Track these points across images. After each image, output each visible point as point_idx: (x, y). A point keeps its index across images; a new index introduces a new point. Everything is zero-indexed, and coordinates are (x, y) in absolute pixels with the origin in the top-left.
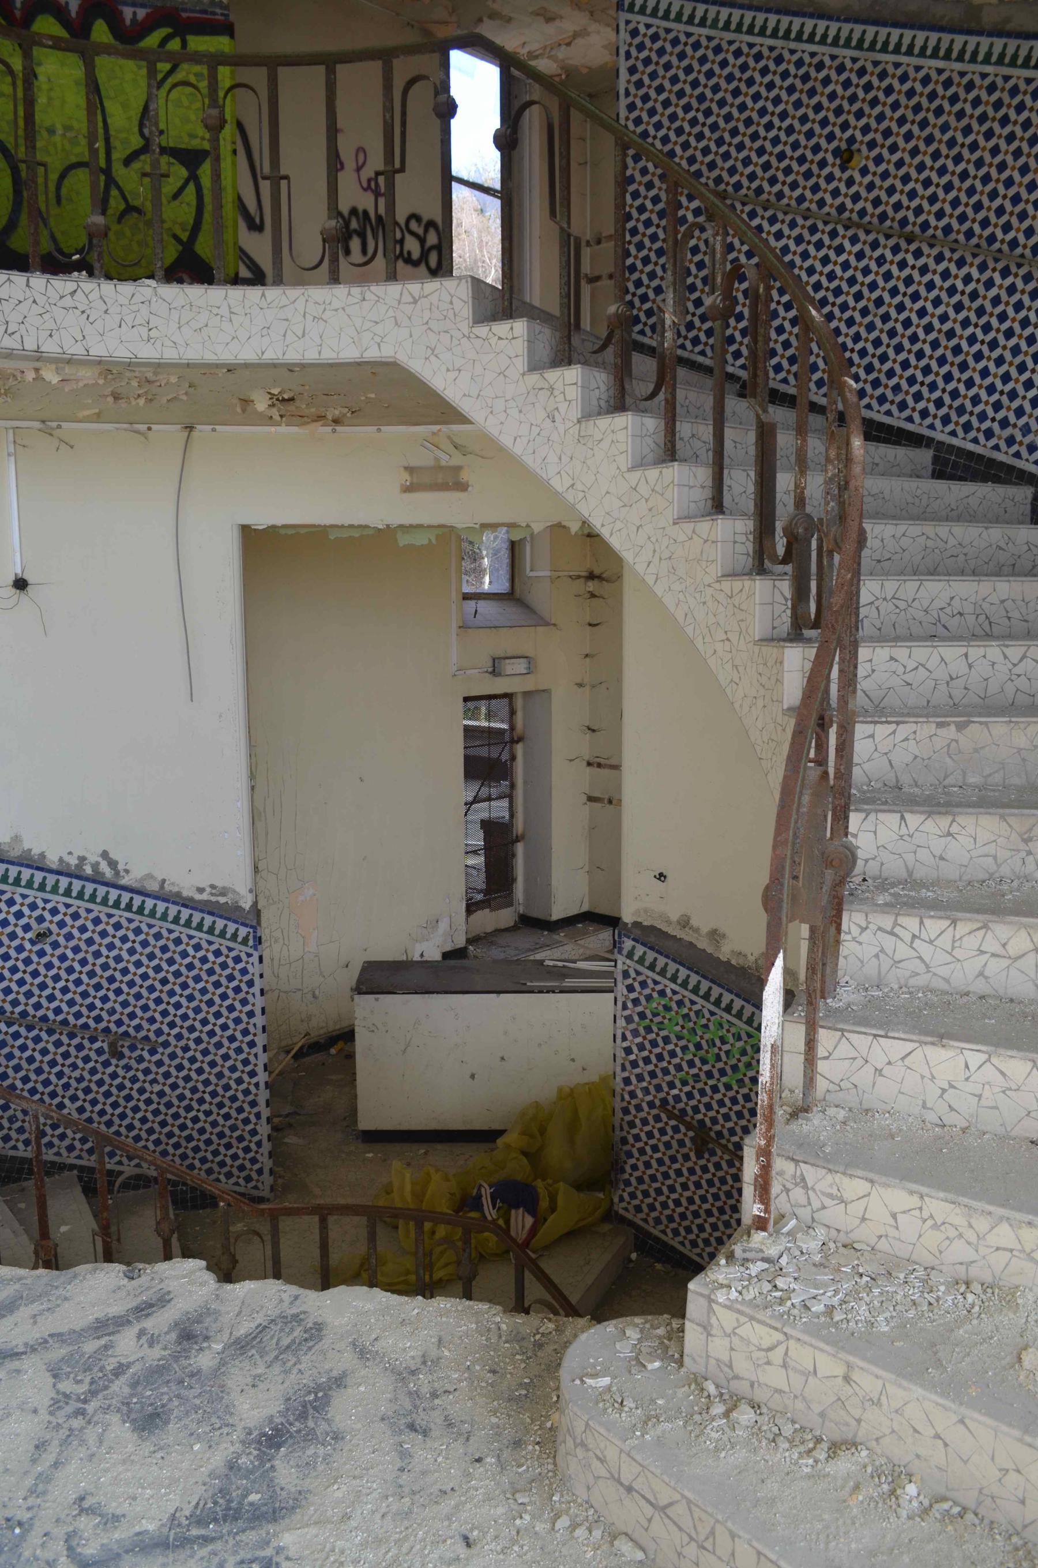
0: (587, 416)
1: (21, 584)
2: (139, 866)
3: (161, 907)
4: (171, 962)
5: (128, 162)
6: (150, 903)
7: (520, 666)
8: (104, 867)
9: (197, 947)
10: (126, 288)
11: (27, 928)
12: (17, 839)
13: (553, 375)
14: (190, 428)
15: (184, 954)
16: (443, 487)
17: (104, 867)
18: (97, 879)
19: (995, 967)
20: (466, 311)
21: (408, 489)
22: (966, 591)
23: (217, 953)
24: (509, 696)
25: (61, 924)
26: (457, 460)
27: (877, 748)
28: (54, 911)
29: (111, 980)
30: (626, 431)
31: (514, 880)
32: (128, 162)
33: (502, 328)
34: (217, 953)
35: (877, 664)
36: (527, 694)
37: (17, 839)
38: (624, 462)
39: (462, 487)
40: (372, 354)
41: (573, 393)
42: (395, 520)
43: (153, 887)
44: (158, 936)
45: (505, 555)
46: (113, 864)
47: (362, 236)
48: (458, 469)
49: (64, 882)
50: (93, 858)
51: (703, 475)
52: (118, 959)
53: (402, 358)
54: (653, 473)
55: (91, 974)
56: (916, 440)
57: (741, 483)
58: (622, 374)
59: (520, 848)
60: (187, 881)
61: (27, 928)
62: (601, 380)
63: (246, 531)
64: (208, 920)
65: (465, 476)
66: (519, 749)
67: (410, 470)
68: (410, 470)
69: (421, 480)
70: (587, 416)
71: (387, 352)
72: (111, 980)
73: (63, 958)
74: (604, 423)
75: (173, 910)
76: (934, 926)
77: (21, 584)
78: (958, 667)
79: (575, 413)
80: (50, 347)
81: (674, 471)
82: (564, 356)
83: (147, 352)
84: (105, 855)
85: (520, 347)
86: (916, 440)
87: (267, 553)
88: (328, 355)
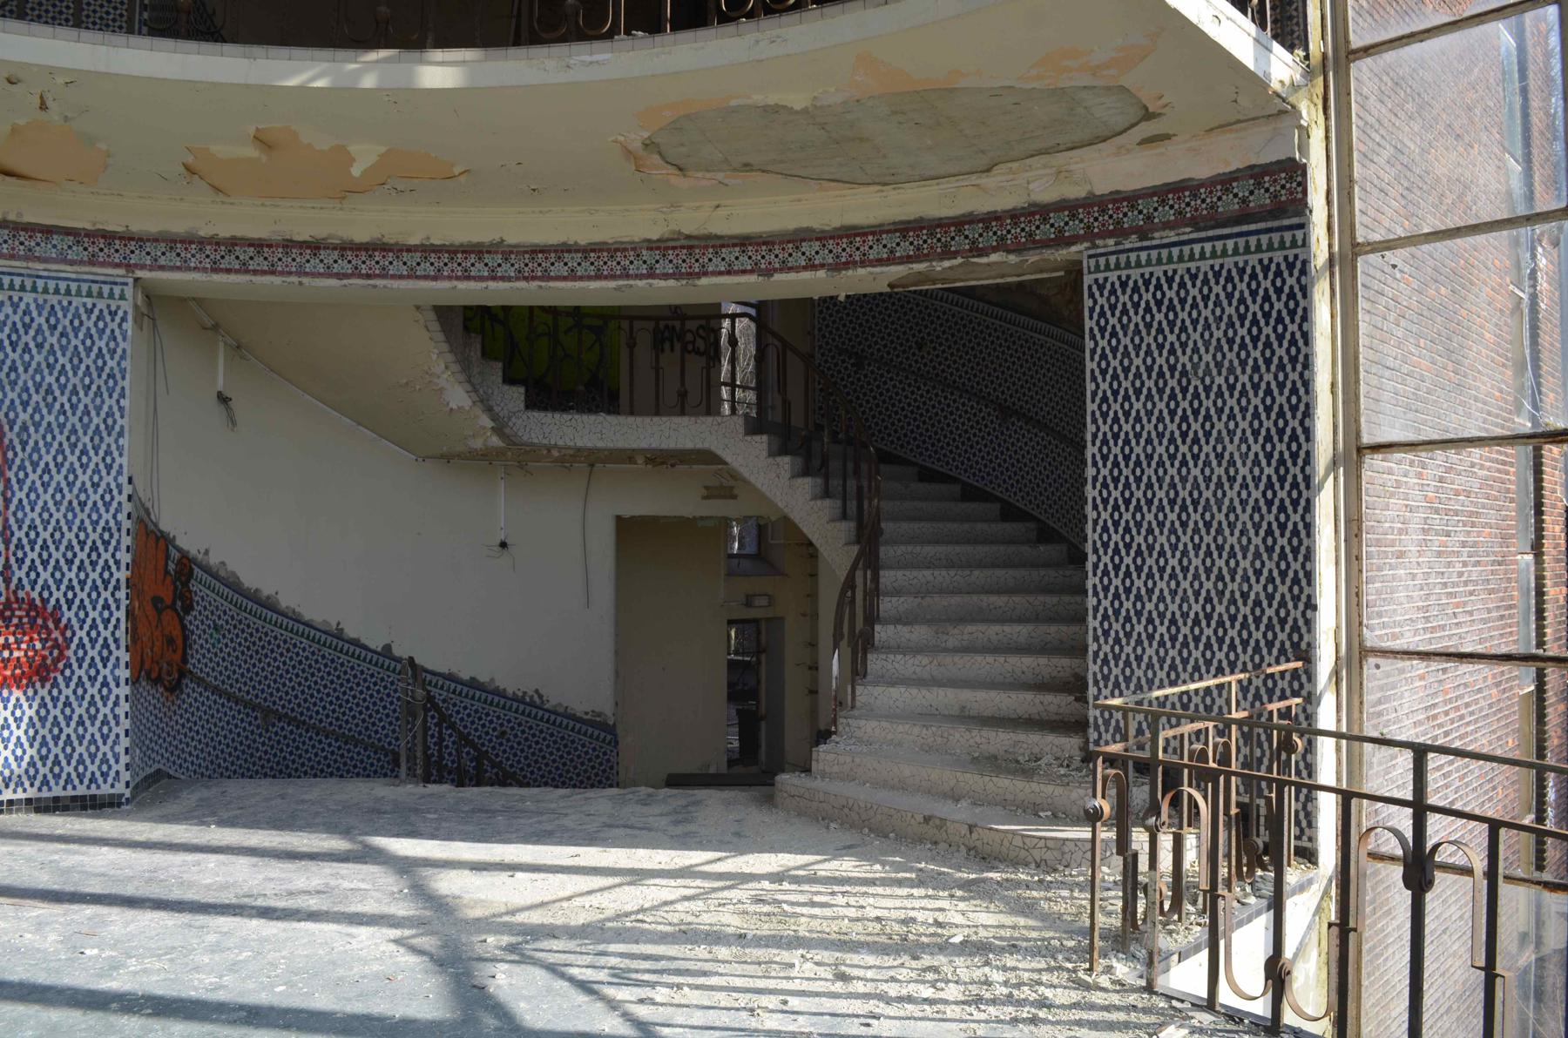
0: (793, 477)
1: (503, 545)
2: (555, 696)
3: (565, 721)
4: (569, 753)
5: (566, 332)
6: (559, 719)
7: (763, 601)
8: (536, 698)
9: (583, 746)
10: (593, 417)
11: (494, 729)
12: (492, 680)
13: (779, 459)
14: (592, 465)
15: (576, 749)
16: (724, 497)
17: (536, 698)
18: (532, 704)
19: (918, 669)
20: (742, 430)
21: (705, 498)
22: (941, 549)
23: (594, 749)
24: (756, 621)
25: (512, 729)
26: (732, 483)
27: (887, 605)
28: (509, 721)
29: (536, 762)
30: (806, 484)
31: (758, 746)
32: (566, 332)
33: (757, 438)
34: (594, 749)
35: (888, 577)
36: (768, 620)
37: (492, 680)
38: (808, 497)
39: (734, 497)
40: (700, 446)
41: (787, 467)
42: (698, 514)
43: (561, 710)
44: (563, 738)
45: (754, 532)
46: (541, 697)
47: (672, 342)
48: (732, 488)
49: (515, 705)
50: (530, 693)
51: (839, 503)
52: (541, 750)
53: (713, 448)
54: (819, 502)
55: (526, 758)
56: (954, 480)
57: (852, 506)
58: (808, 459)
59: (763, 725)
60: (579, 707)
61: (494, 729)
62: (799, 461)
63: (619, 519)
64: (590, 730)
65: (736, 492)
66: (763, 657)
67: (707, 488)
68: (707, 488)
69: (712, 493)
70: (793, 477)
71: (706, 445)
72: (536, 762)
73: (512, 748)
74: (800, 480)
75: (571, 723)
76: (899, 657)
77: (503, 545)
78: (930, 578)
79: (788, 475)
80: (560, 443)
81: (827, 502)
82: (783, 451)
83: (600, 444)
84: (537, 691)
85: (765, 446)
86: (954, 480)
87: (628, 530)
88: (680, 446)
